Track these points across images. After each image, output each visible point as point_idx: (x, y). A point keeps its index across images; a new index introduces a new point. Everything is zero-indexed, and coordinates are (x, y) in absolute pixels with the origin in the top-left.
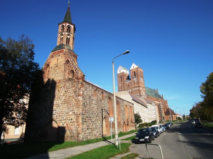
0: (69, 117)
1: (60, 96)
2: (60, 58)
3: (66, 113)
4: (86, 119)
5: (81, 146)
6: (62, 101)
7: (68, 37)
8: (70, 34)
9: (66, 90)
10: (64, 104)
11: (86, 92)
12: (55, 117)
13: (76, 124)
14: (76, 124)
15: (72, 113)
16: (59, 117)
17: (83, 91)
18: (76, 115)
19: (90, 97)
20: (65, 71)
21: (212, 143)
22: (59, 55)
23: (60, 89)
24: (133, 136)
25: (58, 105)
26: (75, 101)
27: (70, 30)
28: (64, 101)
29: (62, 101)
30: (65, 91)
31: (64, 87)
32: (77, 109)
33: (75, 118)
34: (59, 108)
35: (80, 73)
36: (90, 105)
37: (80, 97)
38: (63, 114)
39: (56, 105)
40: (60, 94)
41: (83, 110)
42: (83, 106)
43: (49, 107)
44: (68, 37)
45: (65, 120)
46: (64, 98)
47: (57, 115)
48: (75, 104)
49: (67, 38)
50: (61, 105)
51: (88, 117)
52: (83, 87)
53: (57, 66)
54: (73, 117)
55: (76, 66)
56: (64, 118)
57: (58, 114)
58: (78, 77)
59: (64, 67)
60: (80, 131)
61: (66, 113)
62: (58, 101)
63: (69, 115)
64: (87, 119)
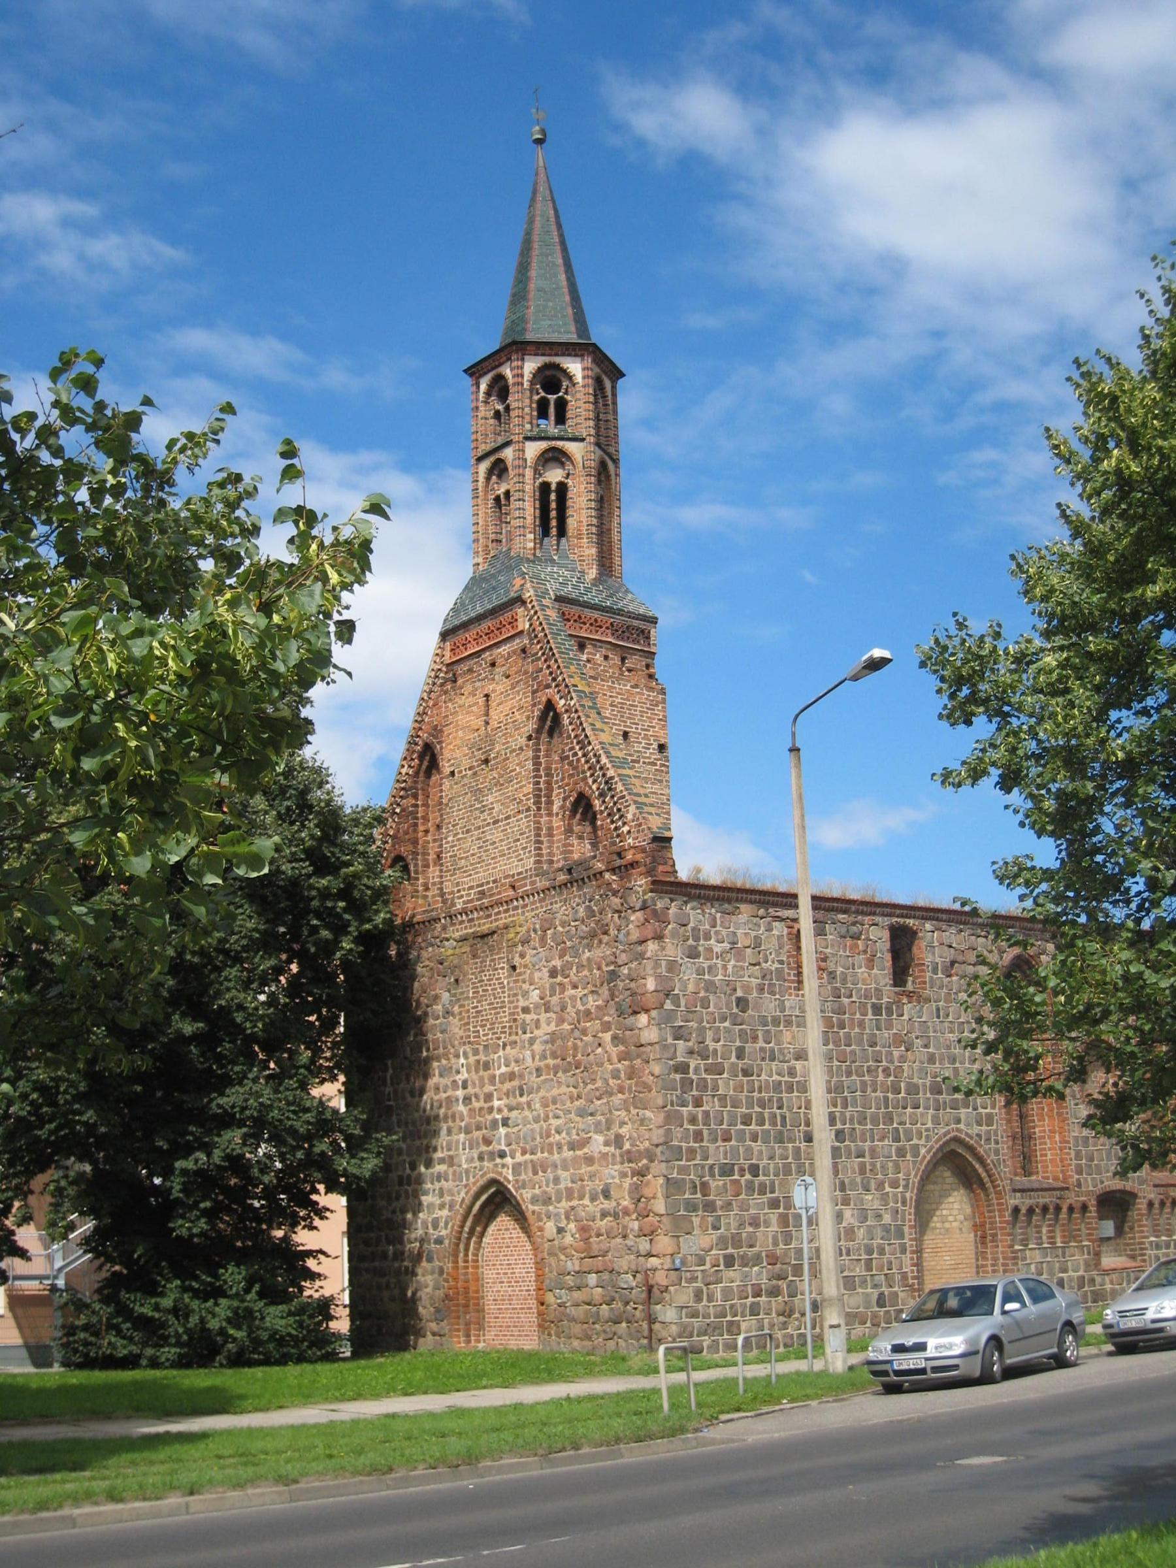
0: (592, 1177)
1: (526, 1010)
2: (498, 687)
3: (572, 1147)
4: (713, 1184)
5: (525, 1402)
6: (538, 1047)
7: (554, 476)
8: (560, 444)
9: (557, 963)
10: (556, 1070)
11: (701, 972)
12: (510, 1178)
13: (636, 1225)
14: (636, 1225)
15: (606, 1144)
16: (535, 1173)
17: (663, 970)
18: (629, 1157)
19: (742, 1003)
20: (542, 798)
21: (2, 1480)
22: (493, 665)
23: (522, 956)
24: (615, 1391)
25: (516, 1083)
26: (614, 1051)
27: (562, 405)
28: (554, 1056)
29: (538, 1047)
30: (553, 973)
31: (543, 940)
32: (634, 1111)
33: (628, 1182)
34: (529, 1104)
35: (630, 816)
36: (746, 1073)
37: (643, 1019)
38: (551, 1152)
39: (507, 1086)
40: (525, 994)
41: (672, 1118)
42: (669, 1087)
43: (467, 1100)
44: (554, 476)
45: (570, 1194)
46: (548, 1026)
47: (519, 1158)
48: (616, 1075)
49: (545, 488)
50: (533, 1080)
51: (727, 1170)
52: (659, 937)
53: (486, 761)
54: (611, 1173)
55: (604, 760)
56: (562, 1186)
57: (524, 1153)
58: (620, 855)
59: (530, 765)
60: (660, 1278)
61: (572, 1147)
62: (514, 1052)
63: (589, 1160)
64: (716, 1183)
